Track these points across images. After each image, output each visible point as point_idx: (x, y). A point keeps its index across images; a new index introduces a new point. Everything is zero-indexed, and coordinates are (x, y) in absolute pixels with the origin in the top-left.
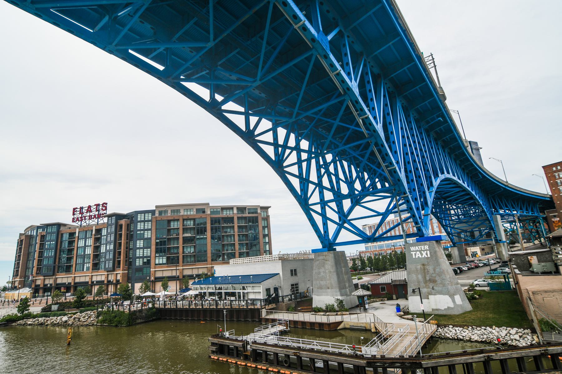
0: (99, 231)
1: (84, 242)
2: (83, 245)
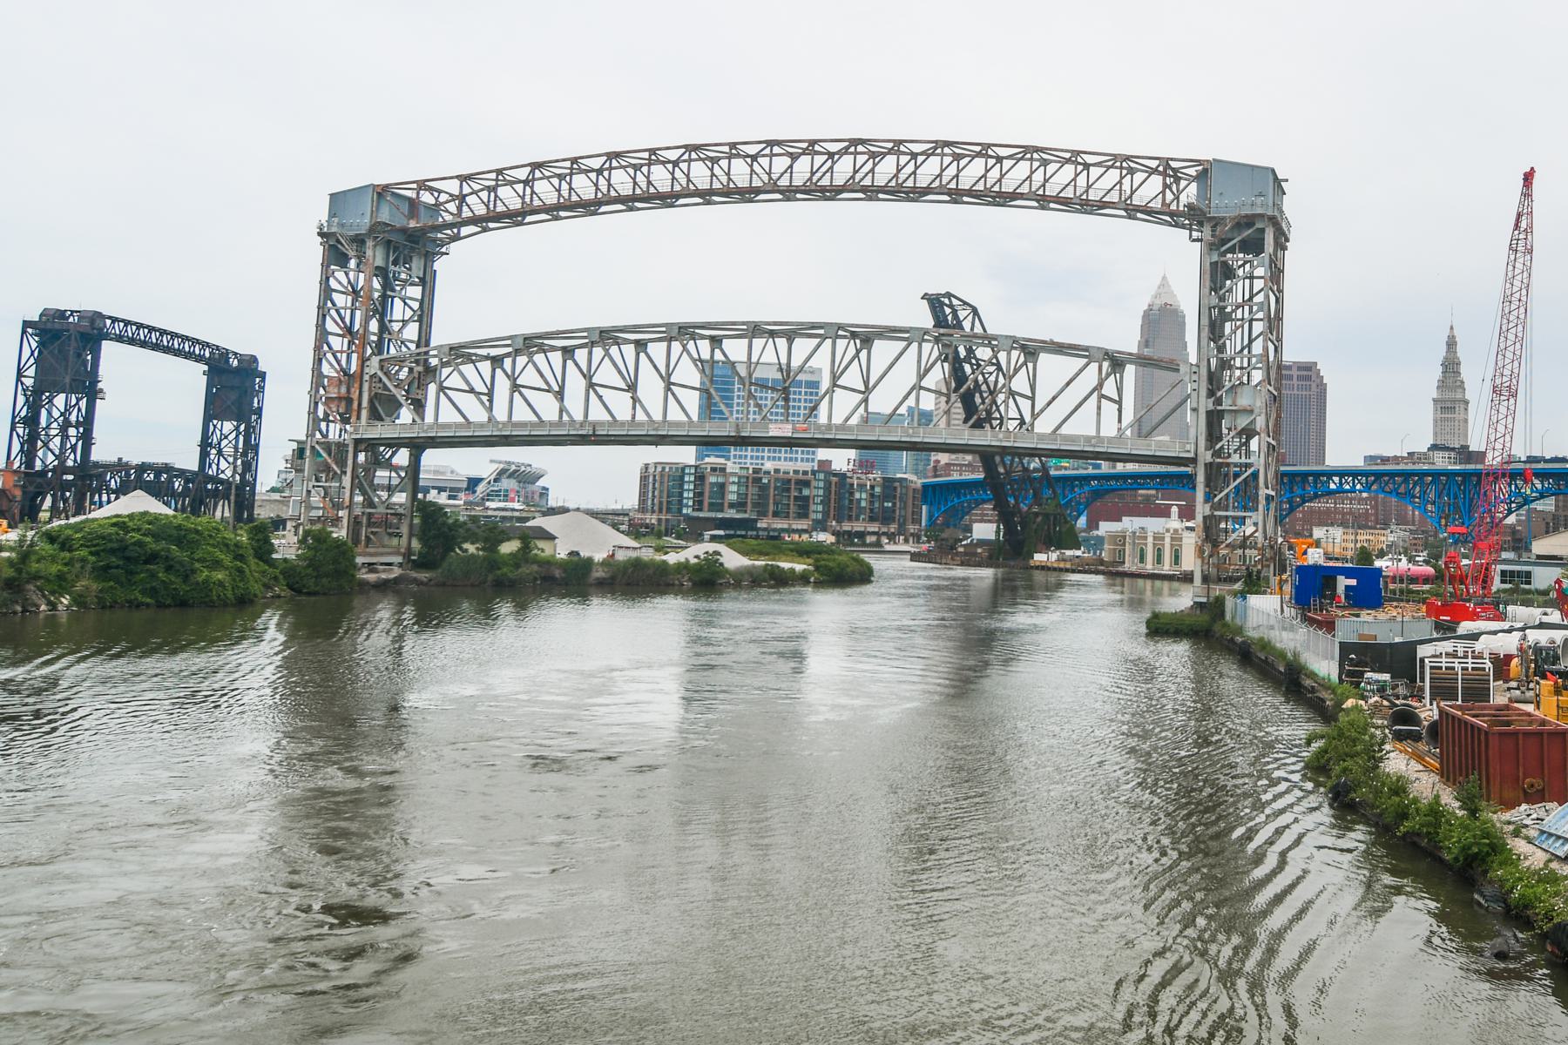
0: (872, 487)
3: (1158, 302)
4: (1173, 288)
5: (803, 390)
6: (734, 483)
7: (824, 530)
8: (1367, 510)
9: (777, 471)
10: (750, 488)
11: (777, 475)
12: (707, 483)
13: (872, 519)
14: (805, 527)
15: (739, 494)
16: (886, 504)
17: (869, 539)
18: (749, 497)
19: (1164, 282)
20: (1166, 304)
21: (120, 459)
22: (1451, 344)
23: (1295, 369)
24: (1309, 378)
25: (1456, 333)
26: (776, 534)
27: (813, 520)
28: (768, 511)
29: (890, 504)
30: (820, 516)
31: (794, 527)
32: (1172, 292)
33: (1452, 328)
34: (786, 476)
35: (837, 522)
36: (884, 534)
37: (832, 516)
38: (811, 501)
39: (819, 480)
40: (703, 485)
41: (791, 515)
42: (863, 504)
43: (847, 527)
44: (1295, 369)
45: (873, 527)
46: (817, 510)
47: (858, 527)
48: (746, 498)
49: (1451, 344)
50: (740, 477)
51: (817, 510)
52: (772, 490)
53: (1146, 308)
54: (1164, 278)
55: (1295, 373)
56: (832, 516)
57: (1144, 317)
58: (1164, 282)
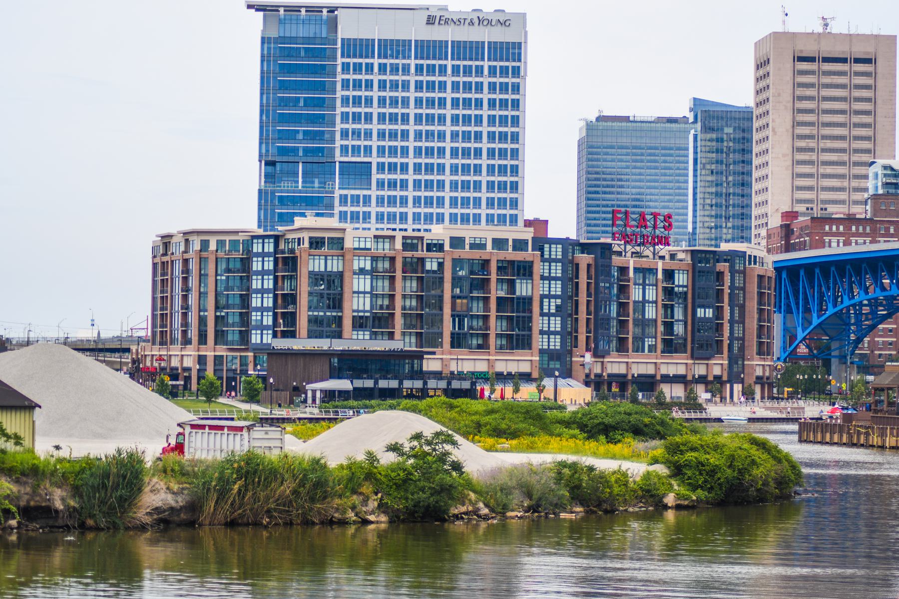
0: (669, 275)
1: (641, 291)
2: (641, 299)
6: (362, 271)
7: (568, 373)
9: (457, 242)
11: (458, 253)
13: (671, 346)
14: (525, 368)
15: (374, 296)
16: (700, 312)
18: (399, 302)
26: (466, 385)
27: (542, 352)
28: (441, 335)
29: (709, 313)
30: (555, 343)
31: (500, 367)
34: (477, 254)
37: (582, 338)
41: (492, 340)
42: (650, 312)
43: (615, 365)
48: (391, 306)
52: (447, 286)
56: (582, 338)
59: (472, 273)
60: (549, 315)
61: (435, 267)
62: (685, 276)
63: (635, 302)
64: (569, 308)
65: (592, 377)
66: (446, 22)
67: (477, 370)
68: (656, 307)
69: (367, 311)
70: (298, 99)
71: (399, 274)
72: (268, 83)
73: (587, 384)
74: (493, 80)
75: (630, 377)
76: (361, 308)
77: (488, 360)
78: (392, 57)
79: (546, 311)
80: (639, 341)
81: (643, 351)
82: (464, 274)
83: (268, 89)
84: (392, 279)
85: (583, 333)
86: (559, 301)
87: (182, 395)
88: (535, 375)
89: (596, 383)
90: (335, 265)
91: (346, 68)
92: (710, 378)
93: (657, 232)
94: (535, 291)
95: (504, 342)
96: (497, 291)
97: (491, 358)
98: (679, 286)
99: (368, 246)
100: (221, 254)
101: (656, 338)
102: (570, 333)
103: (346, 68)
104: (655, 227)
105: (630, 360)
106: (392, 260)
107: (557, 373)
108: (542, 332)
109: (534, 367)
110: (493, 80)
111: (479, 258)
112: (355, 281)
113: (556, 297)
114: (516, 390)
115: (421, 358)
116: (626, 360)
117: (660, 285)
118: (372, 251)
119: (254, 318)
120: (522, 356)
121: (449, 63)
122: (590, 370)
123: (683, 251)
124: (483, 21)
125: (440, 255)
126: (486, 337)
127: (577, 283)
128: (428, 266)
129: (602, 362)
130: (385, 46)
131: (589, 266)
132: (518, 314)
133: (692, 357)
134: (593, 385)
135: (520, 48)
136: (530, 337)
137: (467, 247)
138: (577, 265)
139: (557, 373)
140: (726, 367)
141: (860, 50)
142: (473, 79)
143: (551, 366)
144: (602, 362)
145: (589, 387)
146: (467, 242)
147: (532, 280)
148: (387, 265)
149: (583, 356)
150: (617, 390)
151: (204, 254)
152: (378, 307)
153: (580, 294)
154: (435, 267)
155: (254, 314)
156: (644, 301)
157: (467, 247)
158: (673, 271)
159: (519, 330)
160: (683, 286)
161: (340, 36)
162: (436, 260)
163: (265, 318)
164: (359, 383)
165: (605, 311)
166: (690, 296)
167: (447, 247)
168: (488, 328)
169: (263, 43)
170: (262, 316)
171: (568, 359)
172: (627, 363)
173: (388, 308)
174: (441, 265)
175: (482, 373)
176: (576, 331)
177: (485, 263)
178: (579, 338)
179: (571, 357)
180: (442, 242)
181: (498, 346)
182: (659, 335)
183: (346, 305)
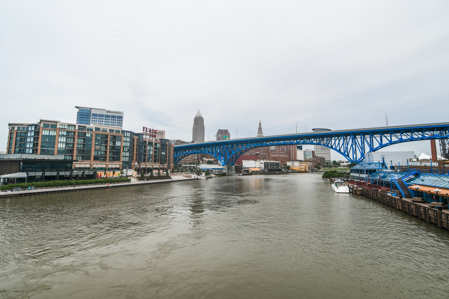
0: (156, 144)
3: (198, 116)
4: (201, 113)
5: (116, 119)
6: (63, 136)
7: (130, 168)
8: (287, 157)
9: (97, 129)
10: (76, 140)
11: (97, 132)
12: (40, 134)
13: (155, 161)
14: (118, 166)
15: (67, 144)
16: (162, 153)
17: (155, 172)
18: (76, 146)
19: (199, 111)
20: (200, 116)
21: (44, 158)
22: (260, 124)
23: (223, 131)
24: (227, 133)
25: (261, 122)
26: (91, 173)
27: (123, 162)
28: (90, 156)
29: (164, 153)
30: (127, 159)
31: (110, 166)
32: (201, 114)
33: (260, 121)
34: (104, 133)
35: (138, 163)
36: (162, 169)
37: (135, 158)
38: (122, 150)
39: (126, 137)
40: (38, 135)
41: (108, 158)
42: (151, 153)
43: (143, 166)
44: (223, 131)
45: (157, 165)
46: (125, 156)
47: (149, 165)
48: (73, 147)
49: (260, 124)
50: (68, 132)
51: (125, 156)
52: (93, 142)
53: (195, 117)
54: (199, 111)
55: (224, 132)
56: (135, 158)
57: (194, 119)
58: (199, 111)
59: (102, 138)
60: (126, 152)
61: (89, 136)
62: (159, 145)
63: (148, 150)
64: (131, 150)
65: (137, 168)
66: (110, 112)
67: (102, 167)
68: (153, 151)
69: (64, 148)
70: (84, 122)
71: (76, 137)
72: (78, 119)
73: (136, 170)
74: (117, 122)
75: (146, 168)
76: (61, 147)
77: (106, 164)
78: (101, 117)
79: (125, 136)
80: (148, 161)
81: (149, 162)
82: (99, 138)
83: (78, 120)
84: (74, 138)
85: (135, 157)
86: (128, 148)
87: (158, 161)
88: (121, 168)
89: (138, 170)
90: (53, 133)
91: (92, 118)
92: (164, 168)
93: (153, 134)
94: (122, 145)
95: (112, 159)
96: (110, 144)
97: (107, 163)
98: (158, 147)
99: (66, 127)
100: (18, 131)
101: (152, 159)
102: (131, 157)
103: (92, 118)
104: (153, 133)
105: (146, 164)
106: (74, 132)
107: (128, 168)
108: (123, 156)
109: (120, 166)
110: (117, 122)
111: (104, 134)
112: (43, 132)
113: (128, 147)
114: (114, 173)
115: (72, 163)
116: (145, 164)
117: (154, 146)
118: (67, 129)
119: (27, 151)
120: (117, 163)
121: (110, 119)
122: (136, 167)
123: (159, 139)
124: (116, 113)
125: (92, 132)
126: (106, 157)
127: (134, 144)
128: (87, 135)
129: (140, 165)
130: (100, 115)
131: (137, 139)
132: (116, 151)
133: (160, 164)
134: (137, 171)
135: (122, 117)
136: (120, 157)
137: (101, 131)
138: (134, 139)
139: (128, 168)
140: (167, 166)
141: (161, 132)
142: (114, 121)
143: (126, 166)
144: (163, 165)
145: (136, 171)
146: (101, 129)
147: (121, 142)
148: (73, 134)
149: (135, 163)
150: (143, 172)
151: (12, 131)
152: (68, 147)
153: (134, 147)
154: (89, 136)
155: (27, 149)
156: (150, 150)
157: (101, 131)
158: (157, 143)
159: (116, 155)
160: (159, 147)
161: (92, 113)
162: (90, 134)
163: (30, 151)
164: (32, 174)
165: (141, 151)
166: (160, 149)
167: (94, 130)
168: (106, 155)
169: (78, 113)
170: (29, 150)
171: (131, 164)
172: (146, 165)
173: (72, 147)
174: (91, 135)
175: (103, 168)
176: (133, 156)
177: (107, 136)
178: (134, 158)
179: (131, 163)
180: (92, 128)
181: (110, 160)
182: (153, 158)
183: (56, 146)
